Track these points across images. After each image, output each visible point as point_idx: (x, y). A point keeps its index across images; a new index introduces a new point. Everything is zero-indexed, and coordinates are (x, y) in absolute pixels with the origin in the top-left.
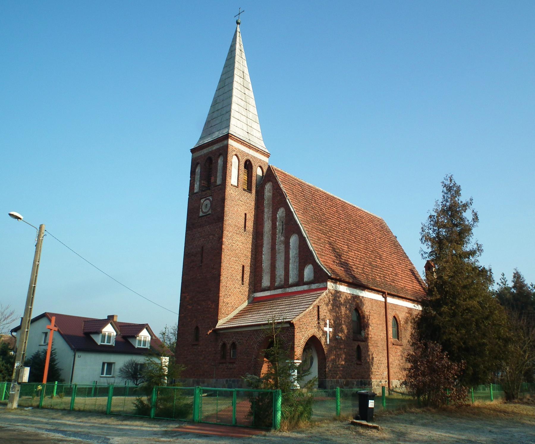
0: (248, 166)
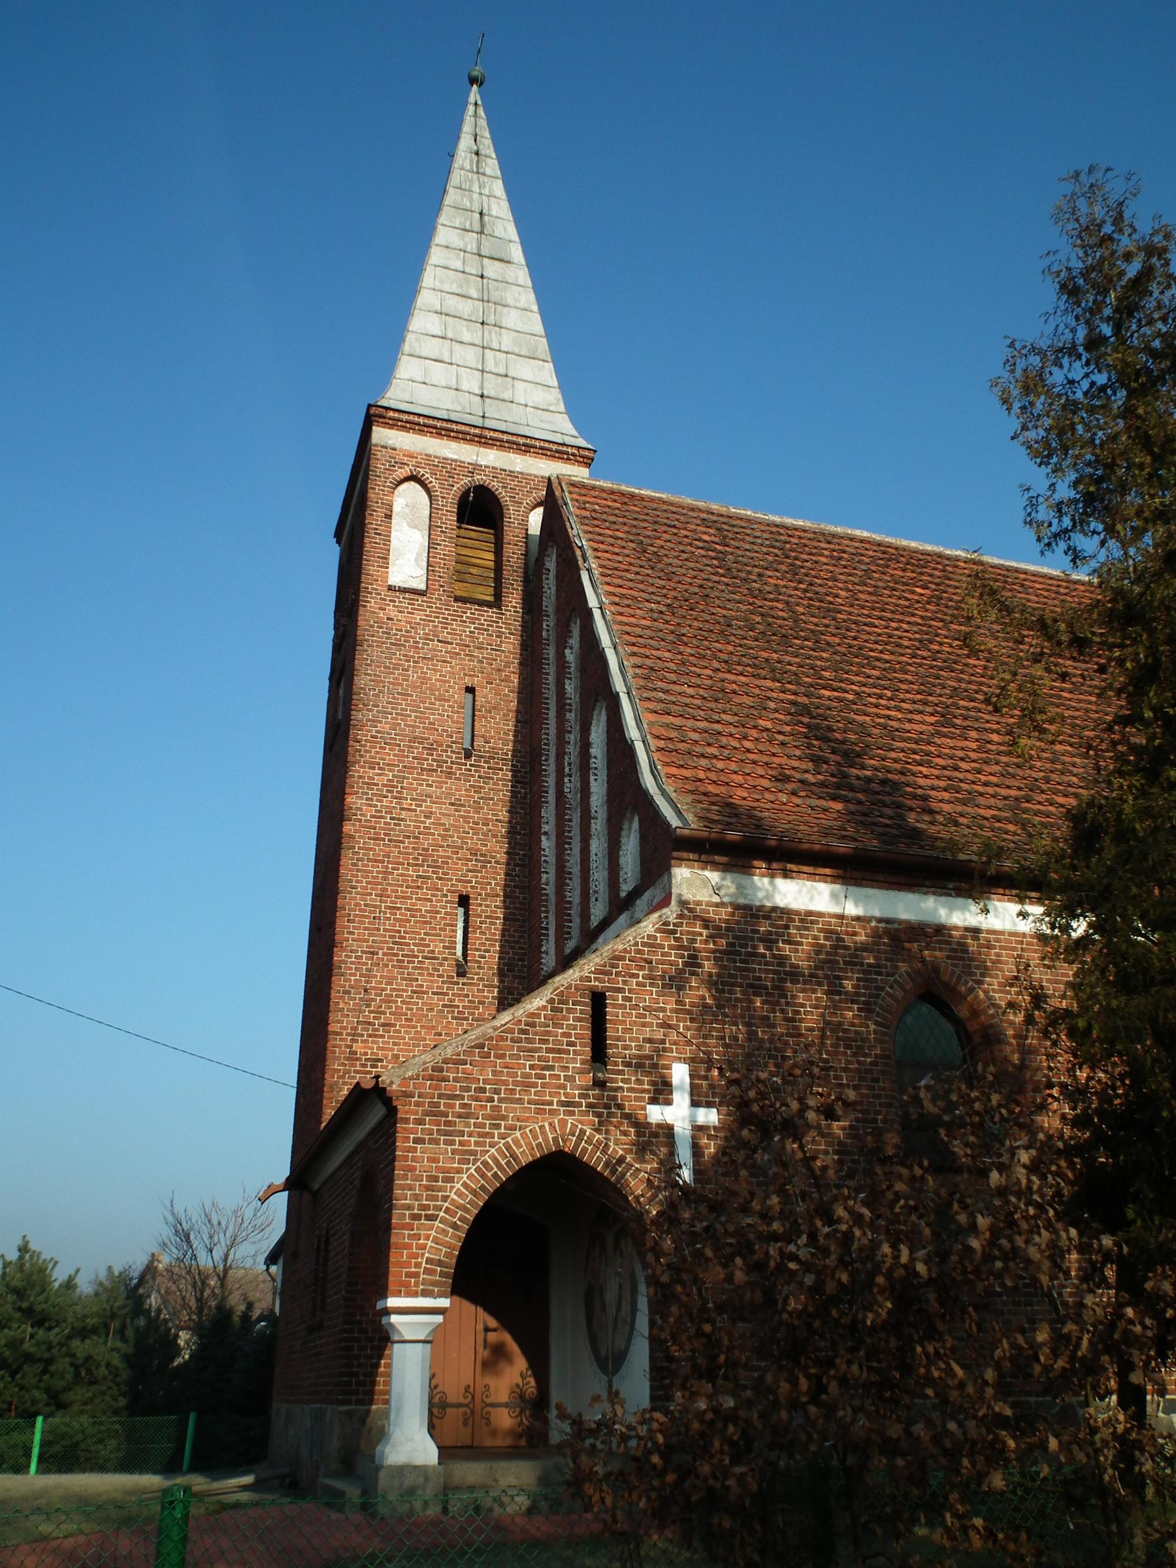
0: (480, 508)
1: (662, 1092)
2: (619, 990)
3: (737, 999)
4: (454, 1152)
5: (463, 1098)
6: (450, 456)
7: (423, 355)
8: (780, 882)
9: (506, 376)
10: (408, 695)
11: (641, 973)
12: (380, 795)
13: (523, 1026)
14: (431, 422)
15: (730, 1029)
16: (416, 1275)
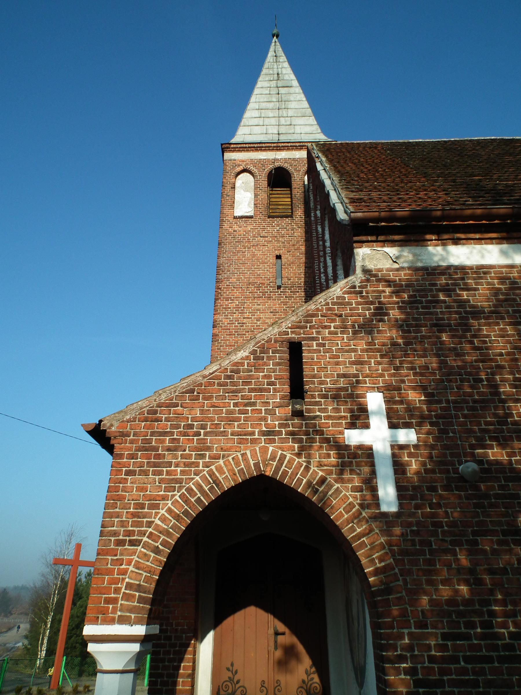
0: (279, 178)
1: (359, 418)
2: (313, 339)
3: (423, 337)
4: (161, 481)
5: (172, 434)
6: (263, 158)
7: (250, 124)
8: (453, 249)
9: (291, 125)
10: (245, 264)
11: (332, 325)
12: (232, 313)
13: (229, 373)
14: (252, 145)
15: (420, 362)
16: (114, 601)
